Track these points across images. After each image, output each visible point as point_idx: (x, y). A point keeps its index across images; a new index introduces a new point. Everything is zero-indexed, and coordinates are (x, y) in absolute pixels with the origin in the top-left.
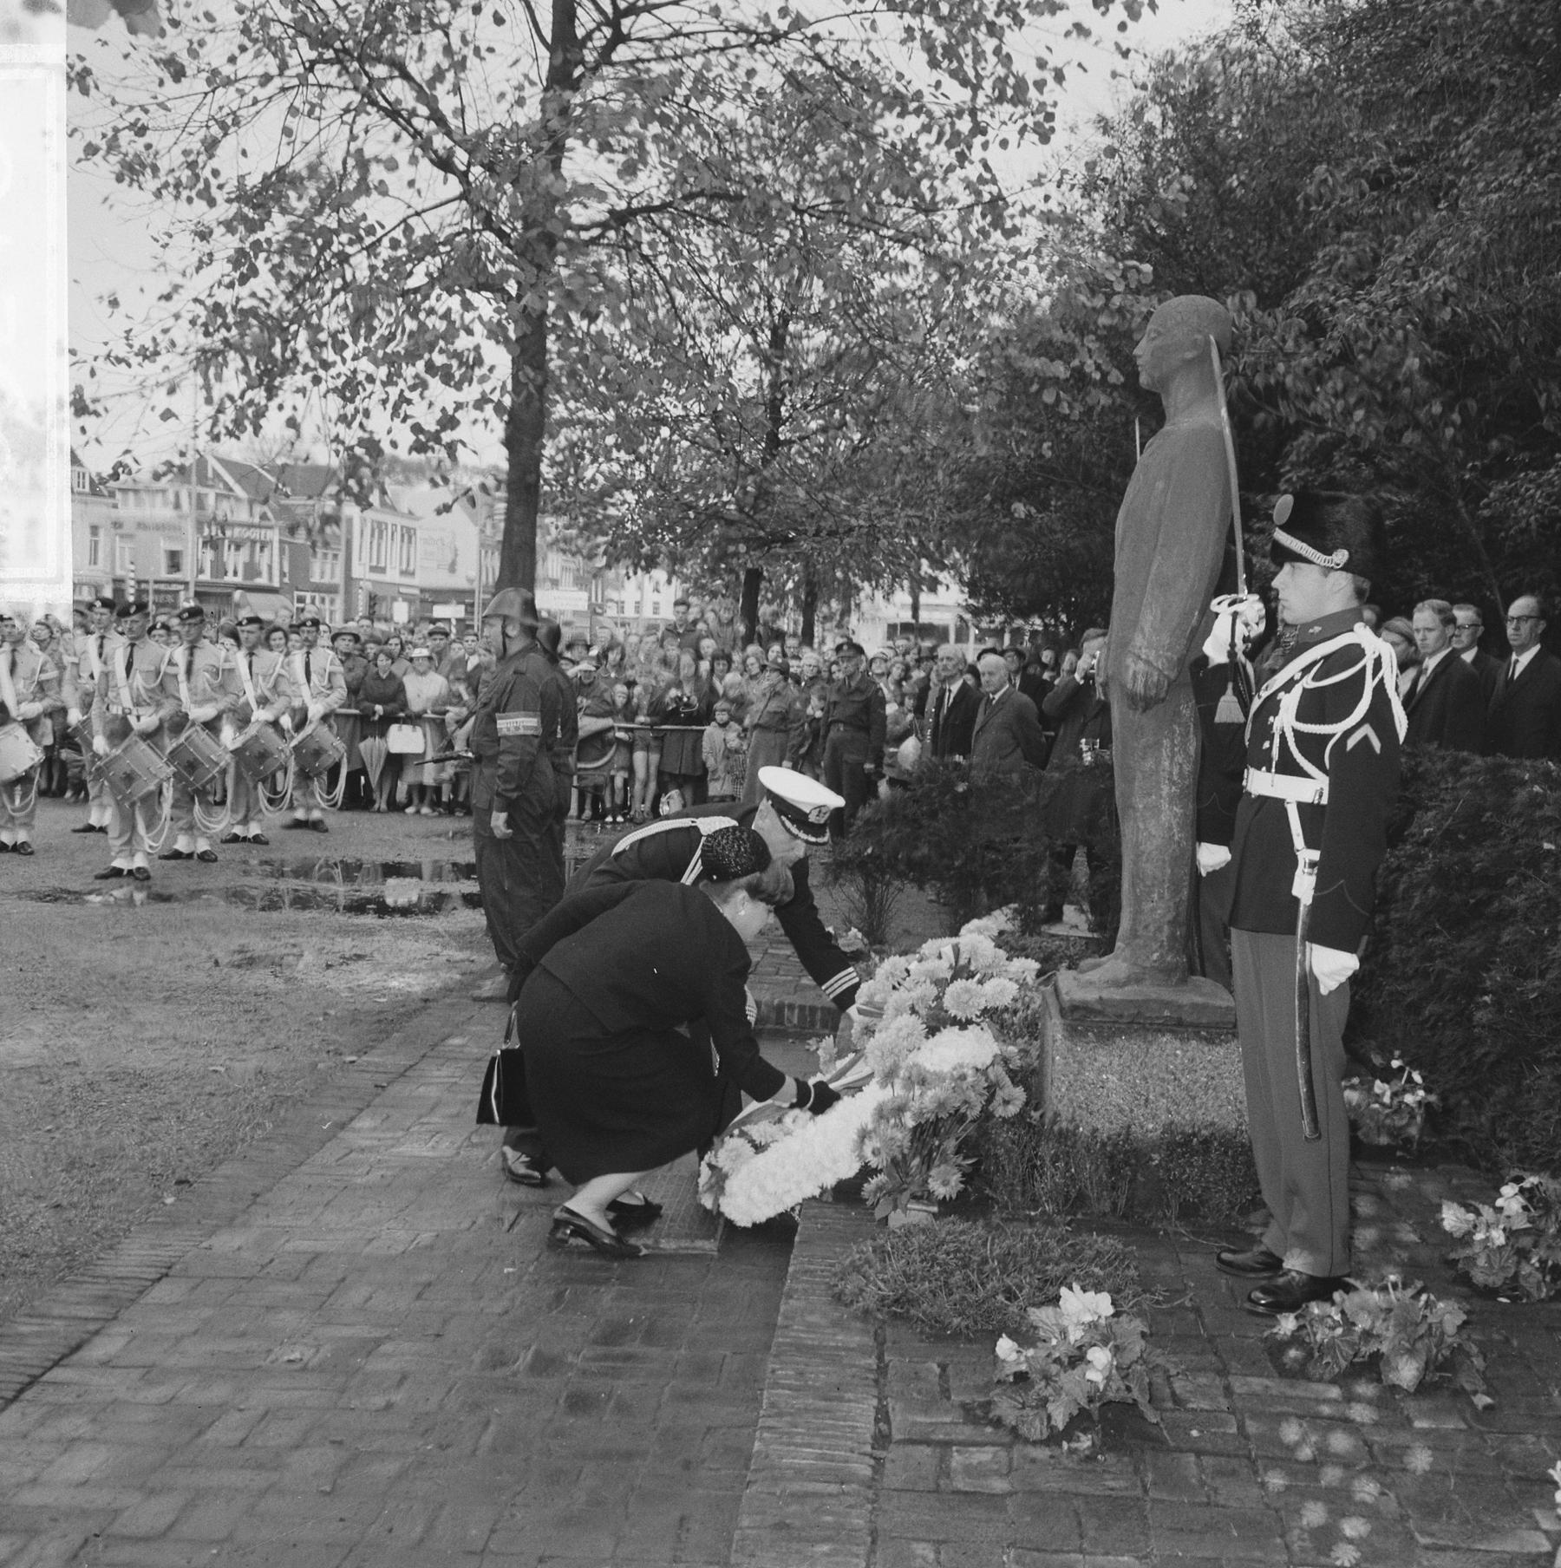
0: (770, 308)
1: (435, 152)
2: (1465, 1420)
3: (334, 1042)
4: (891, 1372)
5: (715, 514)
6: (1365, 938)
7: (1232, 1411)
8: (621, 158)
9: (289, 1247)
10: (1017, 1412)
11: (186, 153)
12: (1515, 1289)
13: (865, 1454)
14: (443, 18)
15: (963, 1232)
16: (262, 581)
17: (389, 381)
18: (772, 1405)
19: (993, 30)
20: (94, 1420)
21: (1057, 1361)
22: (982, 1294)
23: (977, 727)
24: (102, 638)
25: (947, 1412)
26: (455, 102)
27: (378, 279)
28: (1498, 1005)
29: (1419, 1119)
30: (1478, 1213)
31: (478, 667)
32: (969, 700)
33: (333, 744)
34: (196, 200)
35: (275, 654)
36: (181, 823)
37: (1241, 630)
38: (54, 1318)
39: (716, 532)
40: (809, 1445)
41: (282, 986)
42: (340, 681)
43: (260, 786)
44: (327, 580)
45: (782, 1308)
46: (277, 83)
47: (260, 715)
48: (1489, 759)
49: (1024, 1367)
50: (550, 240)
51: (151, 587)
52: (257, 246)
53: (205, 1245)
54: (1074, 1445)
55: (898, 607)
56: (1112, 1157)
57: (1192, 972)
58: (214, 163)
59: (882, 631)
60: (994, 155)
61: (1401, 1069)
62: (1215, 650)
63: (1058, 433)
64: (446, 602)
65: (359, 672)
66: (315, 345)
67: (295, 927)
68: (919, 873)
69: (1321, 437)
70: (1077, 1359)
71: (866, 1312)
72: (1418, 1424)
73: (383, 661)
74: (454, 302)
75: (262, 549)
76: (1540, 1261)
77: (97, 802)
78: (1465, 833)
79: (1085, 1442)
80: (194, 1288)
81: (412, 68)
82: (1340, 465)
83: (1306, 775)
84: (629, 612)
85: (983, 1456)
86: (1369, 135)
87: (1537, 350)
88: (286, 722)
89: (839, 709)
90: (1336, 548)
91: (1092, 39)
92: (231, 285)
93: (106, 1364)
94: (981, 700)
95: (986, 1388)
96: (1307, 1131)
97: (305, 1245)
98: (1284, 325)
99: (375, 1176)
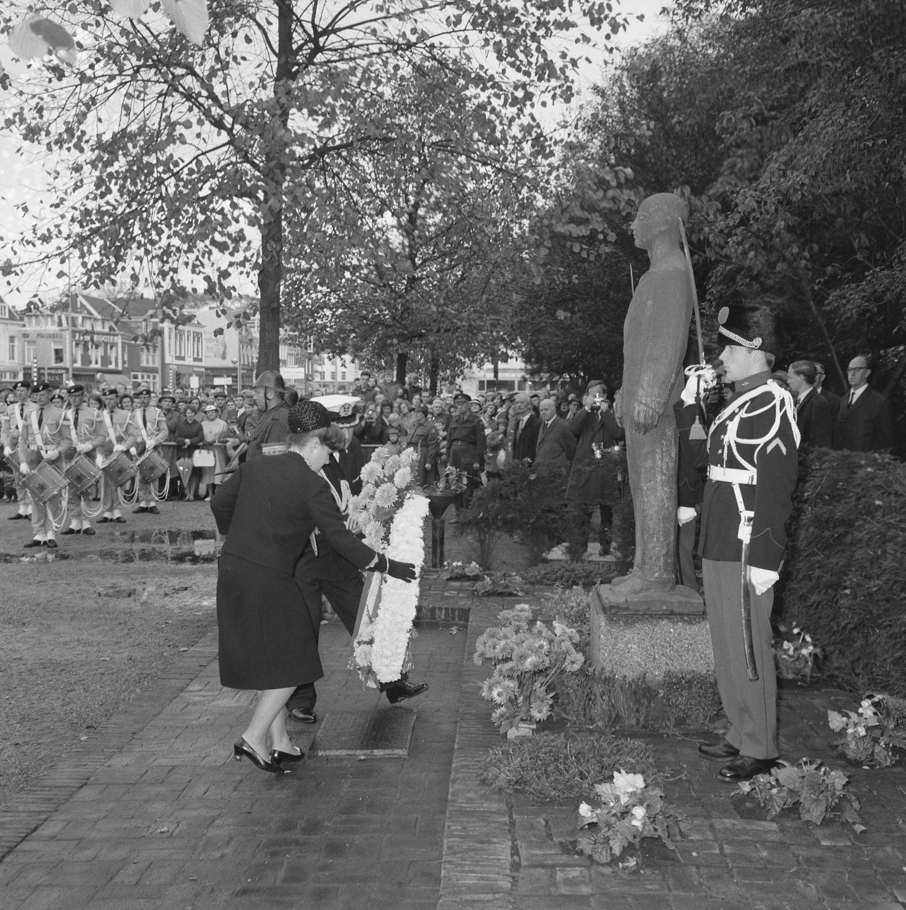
0: (407, 201)
1: (213, 117)
2: (850, 840)
3: (172, 640)
4: (517, 825)
5: (379, 322)
6: (782, 562)
7: (716, 840)
8: (321, 118)
9: (156, 763)
10: (591, 846)
11: (66, 123)
12: (872, 761)
13: (507, 875)
14: (215, 40)
15: (553, 741)
16: (112, 367)
17: (190, 250)
18: (450, 848)
19: (534, 37)
20: (49, 873)
21: (615, 815)
22: (567, 776)
23: (539, 442)
24: (23, 405)
25: (551, 848)
26: (224, 88)
27: (181, 192)
28: (854, 595)
29: (810, 664)
30: (849, 717)
31: (244, 414)
32: (534, 424)
33: (161, 463)
34: (73, 149)
35: (125, 412)
36: (73, 513)
37: (703, 385)
38: (20, 812)
39: (380, 332)
40: (473, 872)
41: (139, 608)
42: (164, 426)
43: (119, 489)
44: (150, 365)
45: (451, 790)
46: (118, 79)
47: (119, 448)
48: (840, 452)
49: (595, 820)
50: (282, 167)
51: (46, 372)
52: (110, 175)
53: (106, 764)
54: (626, 864)
55: (485, 372)
56: (635, 693)
57: (677, 583)
58: (82, 127)
59: (476, 384)
60: (538, 111)
61: (799, 634)
62: (688, 397)
63: (579, 269)
64: (221, 376)
65: (175, 420)
66: (145, 231)
67: (144, 572)
68: (509, 526)
69: (729, 267)
70: (625, 813)
71: (500, 789)
72: (824, 843)
73: (189, 413)
74: (226, 204)
75: (111, 348)
76: (885, 744)
77: (22, 502)
78: (828, 495)
79: (632, 862)
80: (103, 791)
81: (198, 69)
82: (741, 283)
83: (744, 468)
84: (328, 378)
85: (575, 873)
86: (751, 93)
87: (852, 214)
88: (133, 451)
89: (458, 431)
90: (755, 337)
91: (591, 44)
92: (95, 199)
93: (53, 838)
94: (540, 425)
95: (573, 833)
96: (751, 676)
97: (164, 762)
98: (708, 206)
99: (203, 719)
